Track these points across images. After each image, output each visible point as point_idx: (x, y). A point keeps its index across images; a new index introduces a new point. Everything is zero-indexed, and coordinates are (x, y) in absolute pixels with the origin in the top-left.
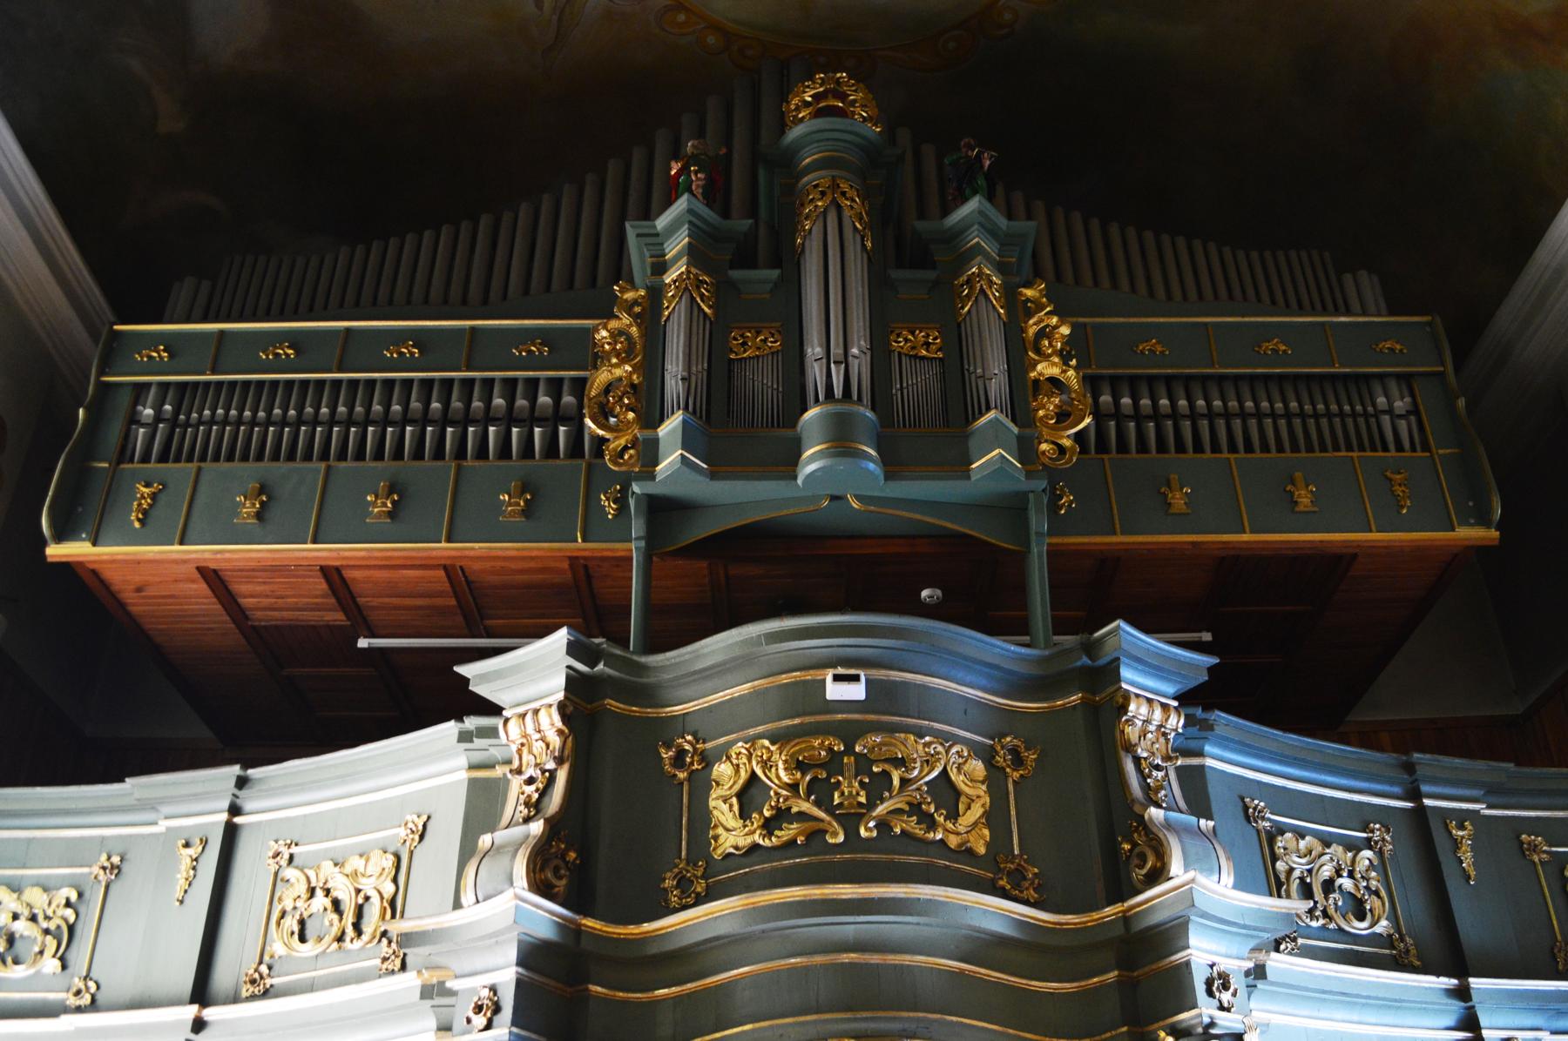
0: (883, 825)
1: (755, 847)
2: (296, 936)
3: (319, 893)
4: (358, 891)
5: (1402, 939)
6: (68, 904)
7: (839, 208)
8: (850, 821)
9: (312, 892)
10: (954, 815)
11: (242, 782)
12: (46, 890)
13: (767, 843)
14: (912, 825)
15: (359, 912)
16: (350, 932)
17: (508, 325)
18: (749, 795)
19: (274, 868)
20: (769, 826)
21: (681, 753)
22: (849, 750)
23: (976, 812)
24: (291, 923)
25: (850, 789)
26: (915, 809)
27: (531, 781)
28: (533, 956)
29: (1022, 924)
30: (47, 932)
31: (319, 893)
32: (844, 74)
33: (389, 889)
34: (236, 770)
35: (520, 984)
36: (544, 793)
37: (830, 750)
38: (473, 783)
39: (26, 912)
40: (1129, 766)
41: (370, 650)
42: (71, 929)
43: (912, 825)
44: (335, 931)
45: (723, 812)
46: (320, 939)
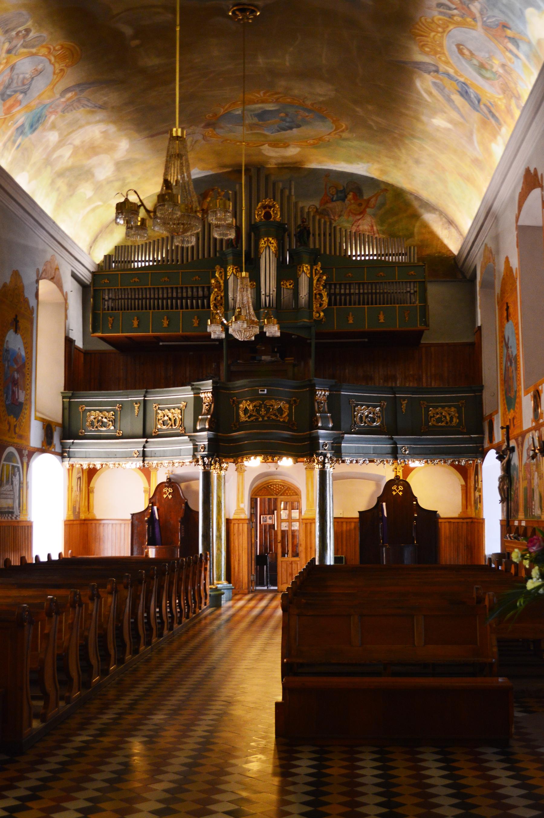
0: (268, 418)
1: (247, 421)
2: (162, 425)
3: (166, 416)
4: (174, 417)
5: (383, 426)
6: (113, 415)
7: (269, 247)
8: (263, 417)
9: (164, 416)
10: (282, 415)
11: (146, 392)
12: (107, 412)
13: (248, 420)
14: (274, 417)
15: (175, 421)
16: (173, 424)
17: (213, 482)
18: (246, 411)
19: (155, 410)
20: (249, 417)
21: (234, 401)
22: (263, 403)
23: (286, 414)
24: (161, 421)
25: (263, 412)
26: (275, 415)
27: (207, 405)
28: (210, 440)
29: (291, 435)
30: (109, 421)
31: (166, 416)
32: (255, 283)
33: (180, 417)
34: (145, 390)
35: (208, 444)
36: (210, 408)
37: (260, 403)
38: (194, 397)
39: (104, 417)
40: (316, 404)
41: (163, 345)
42: (114, 420)
43: (274, 417)
44: (170, 424)
45: (241, 414)
46: (167, 425)
